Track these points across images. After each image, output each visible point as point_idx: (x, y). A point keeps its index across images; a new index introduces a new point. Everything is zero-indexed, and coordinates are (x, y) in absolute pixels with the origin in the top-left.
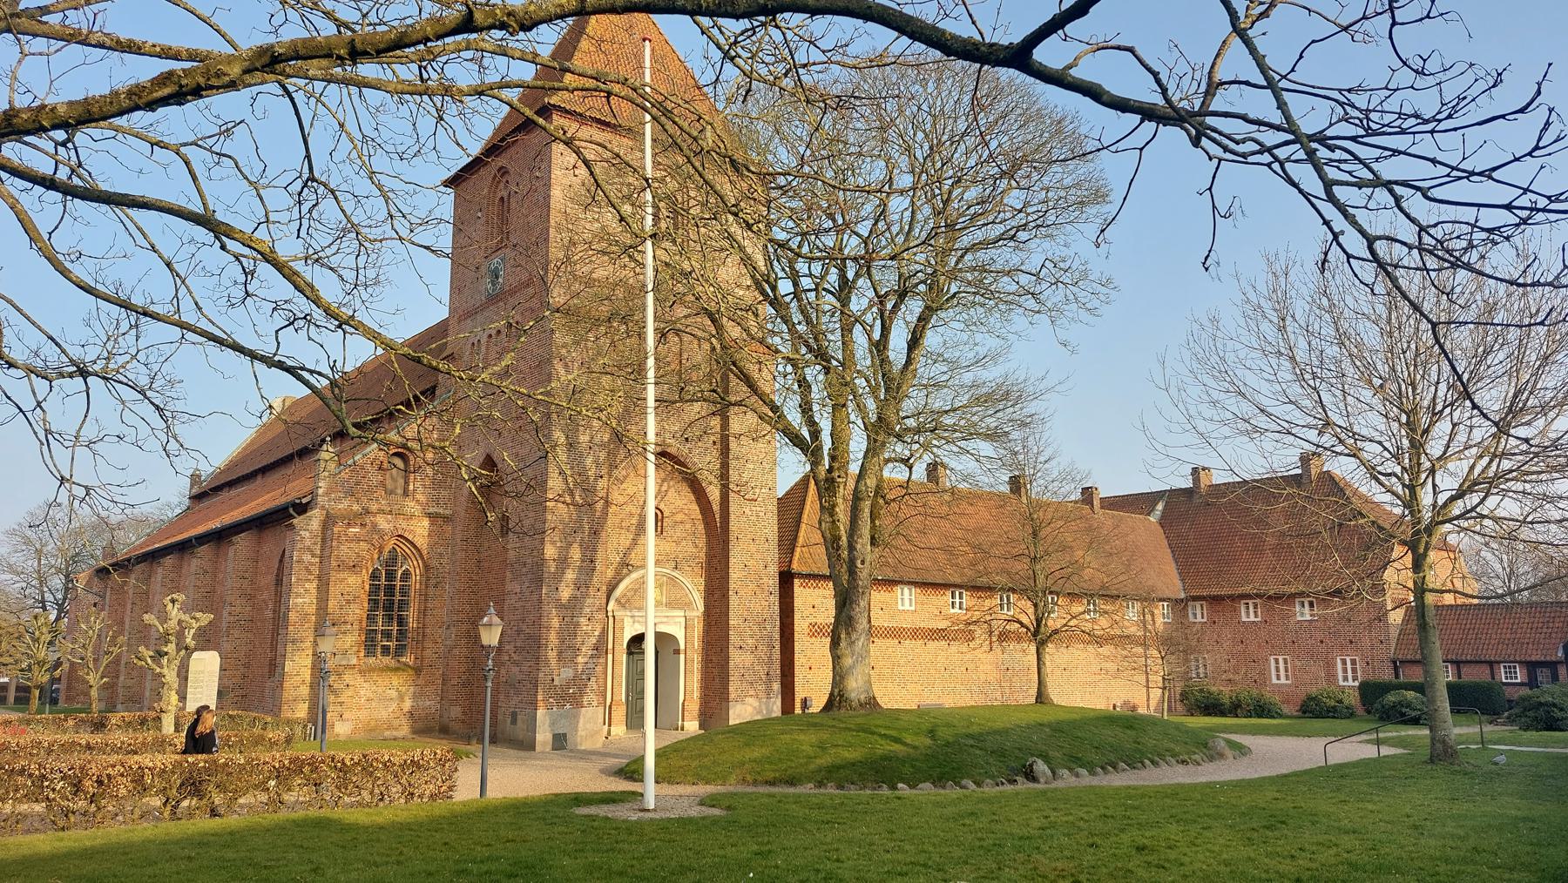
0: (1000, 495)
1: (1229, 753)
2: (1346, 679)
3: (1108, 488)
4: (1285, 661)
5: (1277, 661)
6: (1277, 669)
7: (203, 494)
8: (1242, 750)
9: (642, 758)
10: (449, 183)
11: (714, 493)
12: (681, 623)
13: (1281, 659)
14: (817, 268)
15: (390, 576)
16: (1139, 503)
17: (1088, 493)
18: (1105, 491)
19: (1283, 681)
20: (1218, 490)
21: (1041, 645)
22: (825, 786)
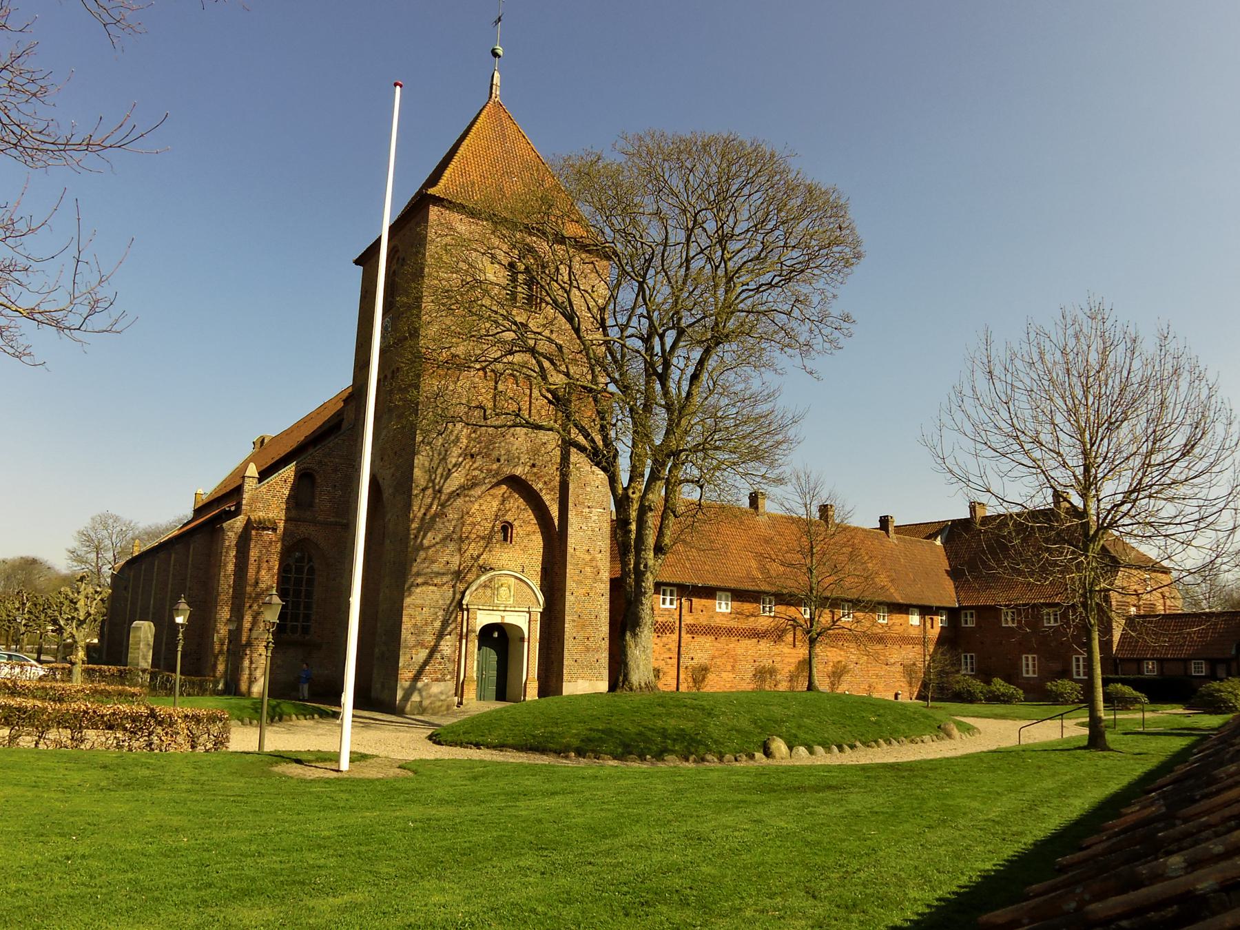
0: (809, 523)
1: (955, 732)
2: (1027, 672)
3: (900, 519)
4: (1034, 659)
5: (1027, 659)
6: (1027, 665)
7: (198, 512)
8: (969, 729)
9: (356, 706)
10: (357, 262)
11: (554, 511)
12: (523, 616)
13: (1030, 657)
14: (488, 325)
15: (299, 570)
16: (929, 531)
17: (884, 522)
18: (898, 521)
19: (1031, 675)
20: (986, 520)
21: (812, 642)
22: (1174, 826)
